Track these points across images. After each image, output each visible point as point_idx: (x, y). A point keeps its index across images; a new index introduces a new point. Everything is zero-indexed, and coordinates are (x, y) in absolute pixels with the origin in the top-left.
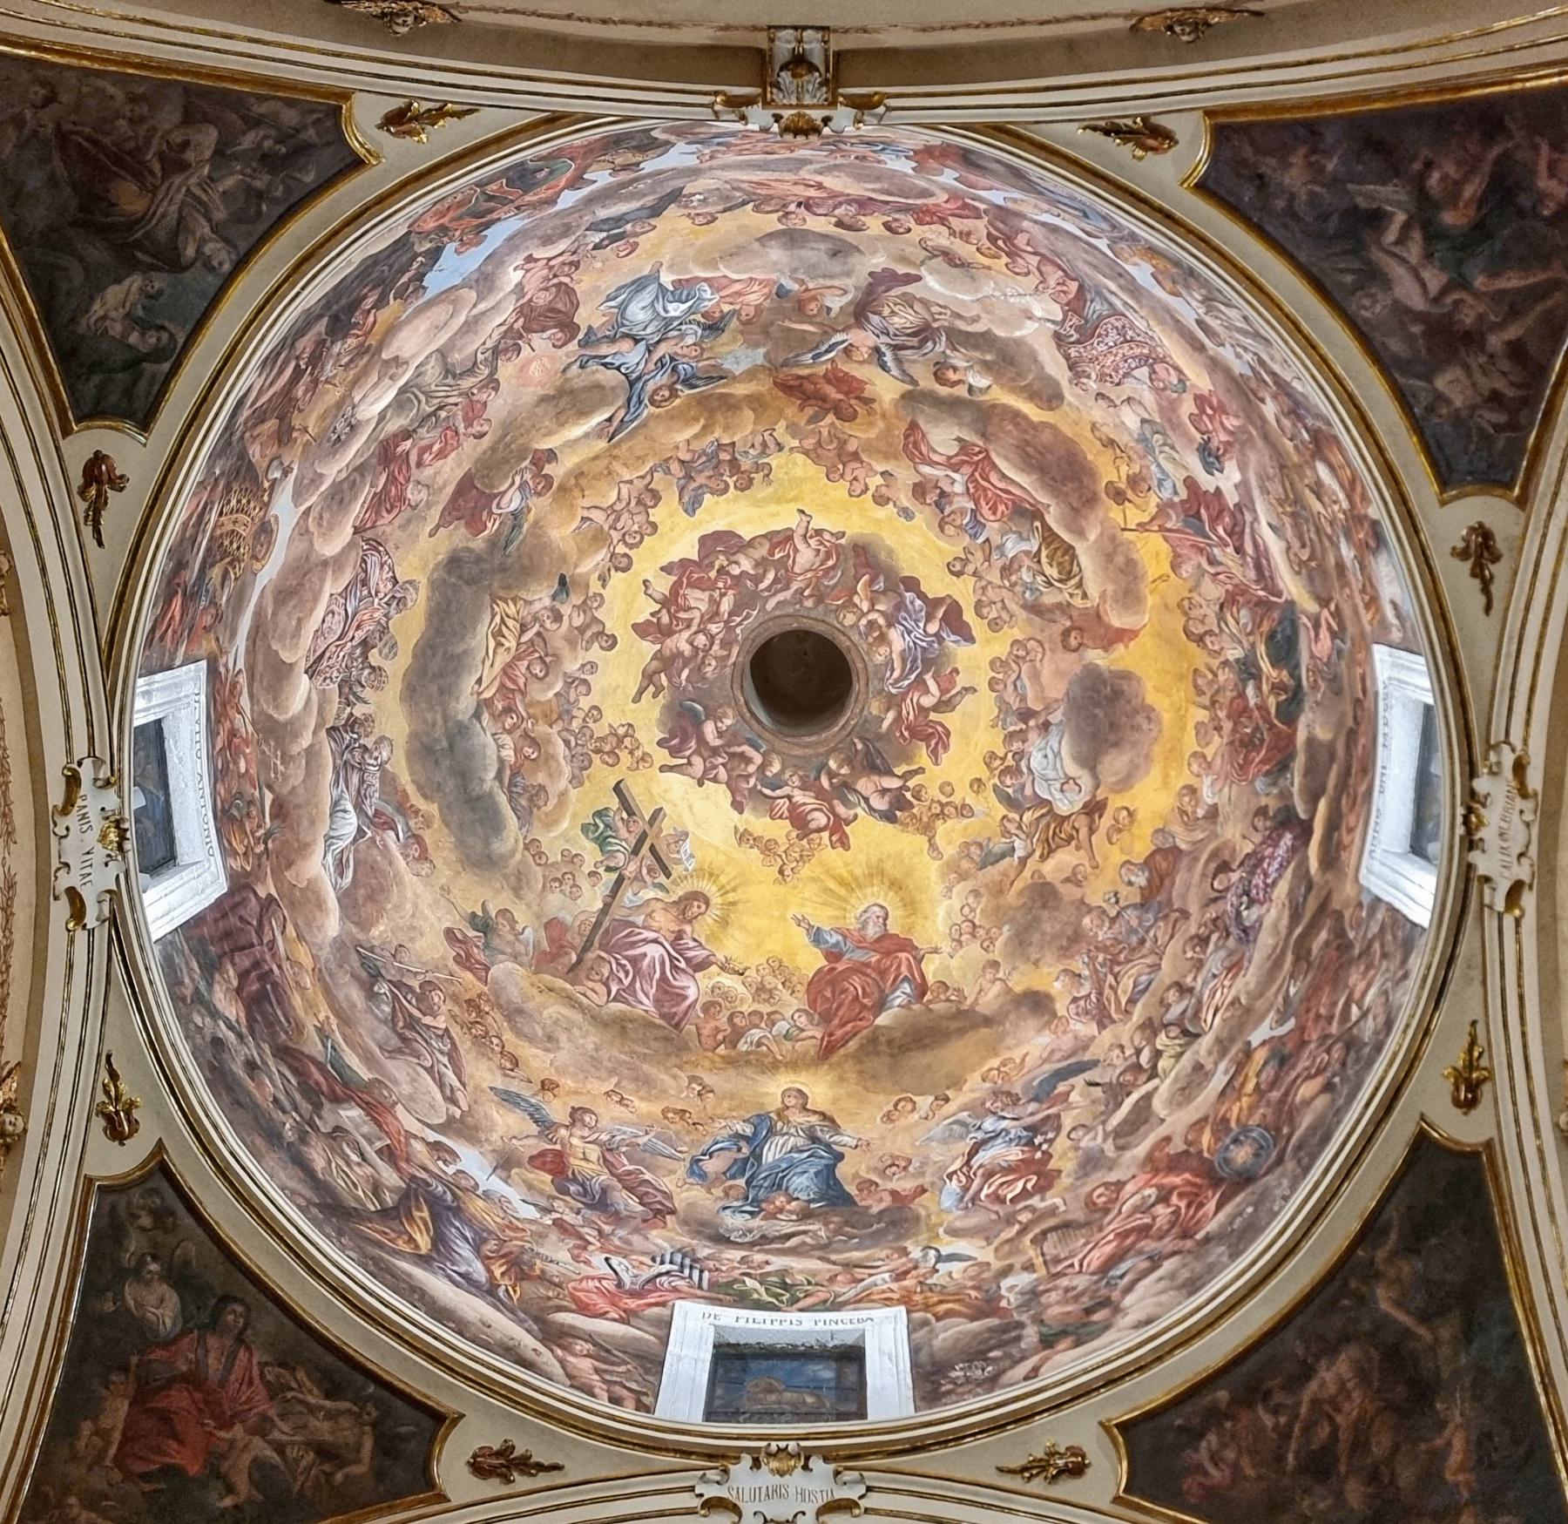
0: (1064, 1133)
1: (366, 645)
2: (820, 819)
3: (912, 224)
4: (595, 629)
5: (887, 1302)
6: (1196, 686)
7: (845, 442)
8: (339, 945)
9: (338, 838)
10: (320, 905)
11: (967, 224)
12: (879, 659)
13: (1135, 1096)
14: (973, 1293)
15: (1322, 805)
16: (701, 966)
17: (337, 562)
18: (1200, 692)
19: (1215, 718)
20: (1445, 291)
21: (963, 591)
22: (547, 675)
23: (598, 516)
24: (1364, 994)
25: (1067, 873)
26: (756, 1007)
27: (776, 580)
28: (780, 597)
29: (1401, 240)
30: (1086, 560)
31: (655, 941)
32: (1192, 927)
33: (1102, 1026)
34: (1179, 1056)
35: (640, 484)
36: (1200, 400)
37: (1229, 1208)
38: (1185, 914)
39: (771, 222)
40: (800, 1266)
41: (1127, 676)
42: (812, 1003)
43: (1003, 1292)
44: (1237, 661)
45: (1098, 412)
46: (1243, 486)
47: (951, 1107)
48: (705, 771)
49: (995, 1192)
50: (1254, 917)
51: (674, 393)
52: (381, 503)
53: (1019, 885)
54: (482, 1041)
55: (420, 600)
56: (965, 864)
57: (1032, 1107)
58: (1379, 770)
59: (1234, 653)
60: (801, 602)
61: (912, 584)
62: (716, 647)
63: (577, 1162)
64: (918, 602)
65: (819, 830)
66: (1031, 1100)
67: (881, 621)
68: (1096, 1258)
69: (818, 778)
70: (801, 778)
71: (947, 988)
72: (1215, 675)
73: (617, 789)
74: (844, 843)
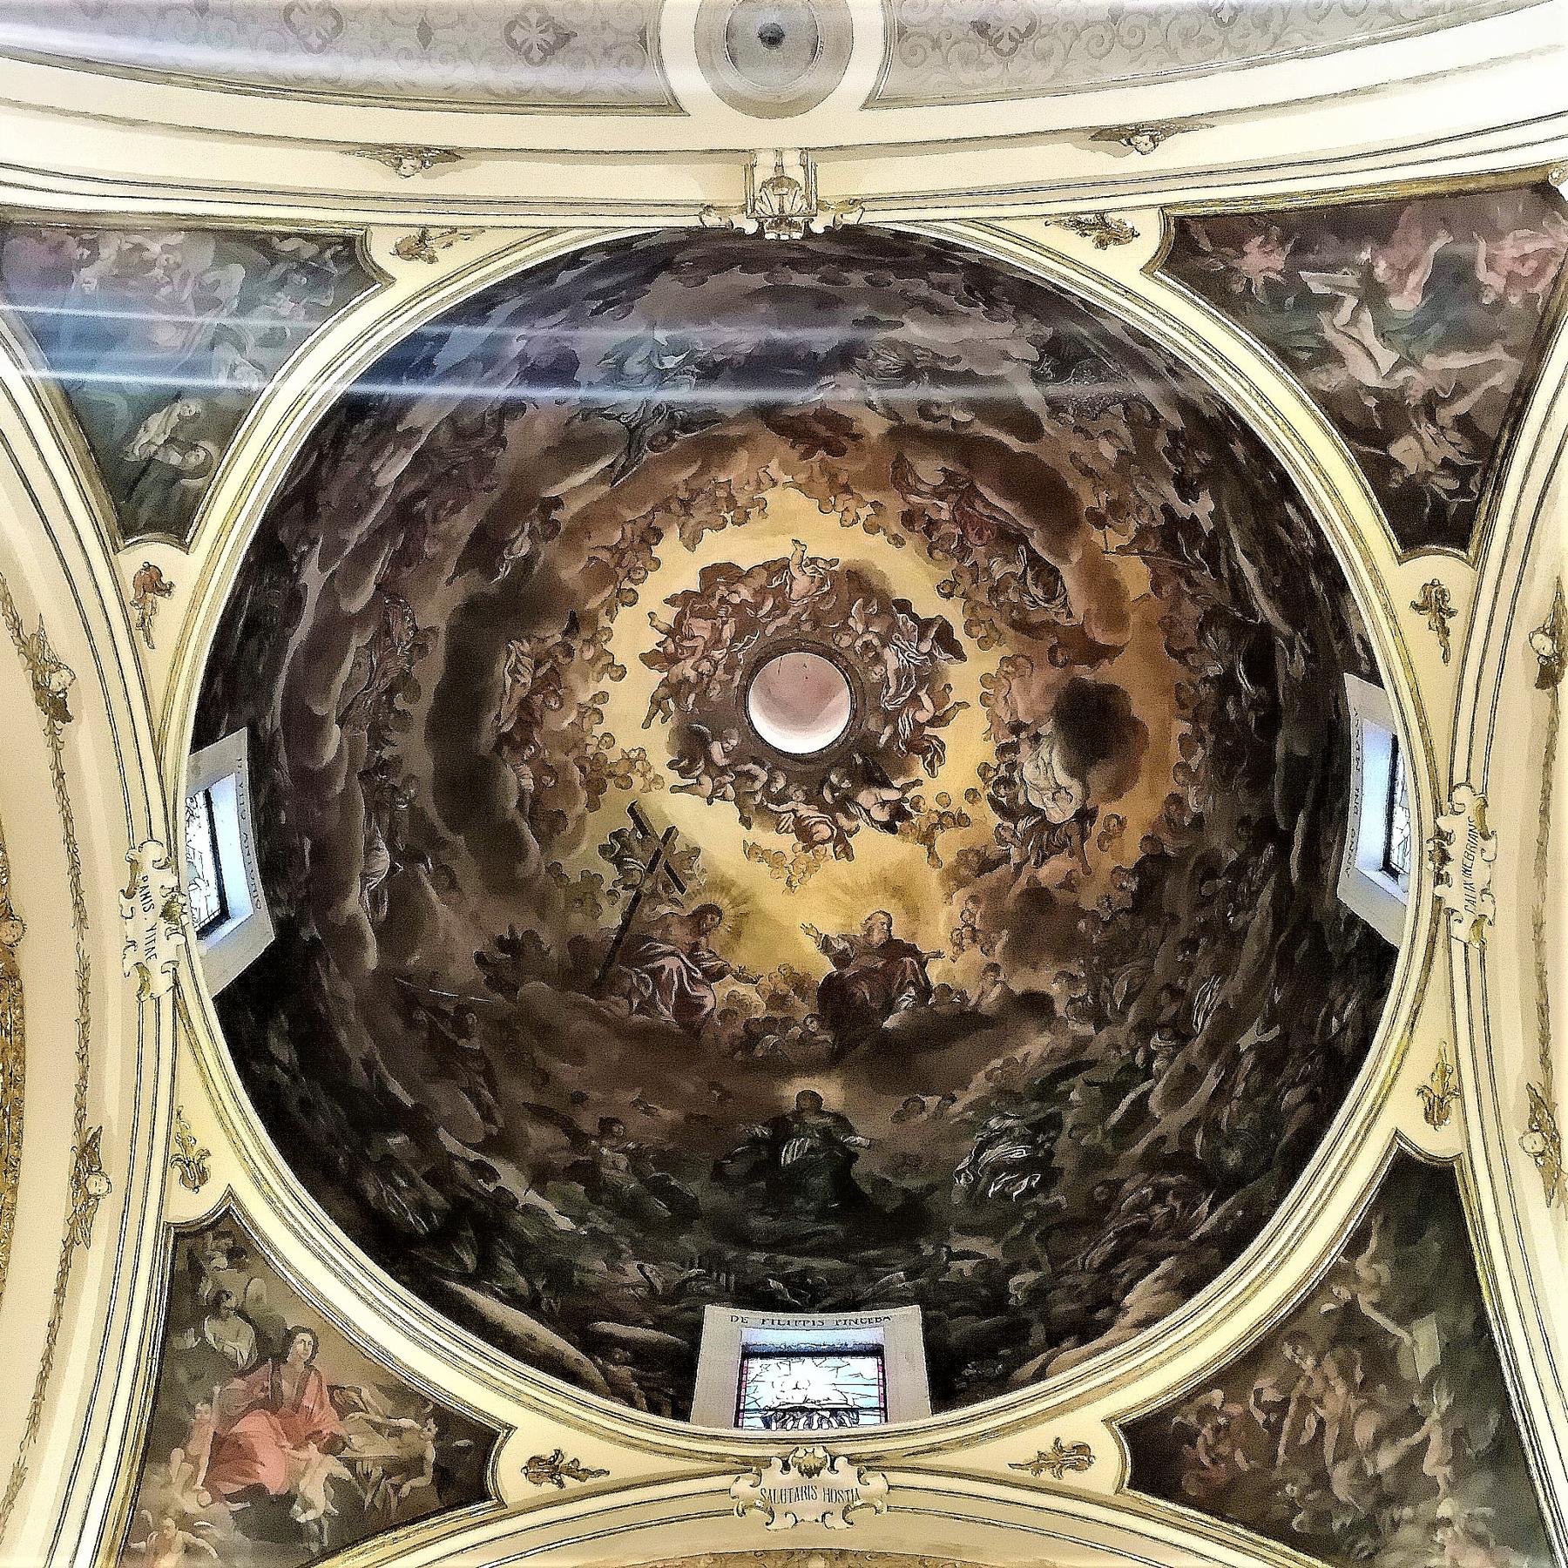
0: (1066, 1132)
1: (391, 691)
2: (824, 831)
3: (892, 278)
4: (605, 660)
5: (903, 1301)
6: (1178, 699)
7: (836, 476)
8: (378, 975)
9: (373, 874)
10: (360, 939)
11: (947, 276)
12: (875, 678)
13: (1132, 1096)
14: (984, 1292)
15: (1301, 819)
16: (719, 975)
17: (361, 618)
18: (1183, 706)
19: (1197, 730)
20: (1397, 366)
21: (953, 613)
22: (562, 705)
23: (604, 556)
24: (1344, 1006)
25: (1061, 879)
26: (772, 1013)
27: (774, 607)
28: (779, 622)
29: (1354, 320)
30: (1070, 579)
31: (672, 954)
32: (1183, 932)
33: (1098, 1028)
34: (1171, 1058)
35: (643, 524)
36: (1174, 436)
37: (1220, 1211)
38: (1175, 919)
39: (758, 280)
40: (822, 1265)
41: (1112, 690)
42: (822, 1007)
43: (1012, 1291)
44: (1218, 677)
45: (1077, 445)
46: (1216, 515)
47: (957, 1108)
48: (714, 790)
49: (1002, 1191)
50: (1240, 924)
51: (672, 439)
52: (402, 559)
53: (1016, 890)
54: (516, 1061)
55: (438, 650)
56: (964, 872)
57: (1034, 1106)
58: (1353, 791)
59: (1214, 670)
60: (798, 626)
61: (904, 606)
62: (720, 672)
63: (608, 1172)
64: (910, 623)
65: (823, 842)
66: (1033, 1100)
67: (876, 642)
68: (1097, 1256)
69: (820, 792)
70: (806, 793)
71: (951, 991)
72: (1196, 689)
73: (631, 810)
74: (848, 853)
